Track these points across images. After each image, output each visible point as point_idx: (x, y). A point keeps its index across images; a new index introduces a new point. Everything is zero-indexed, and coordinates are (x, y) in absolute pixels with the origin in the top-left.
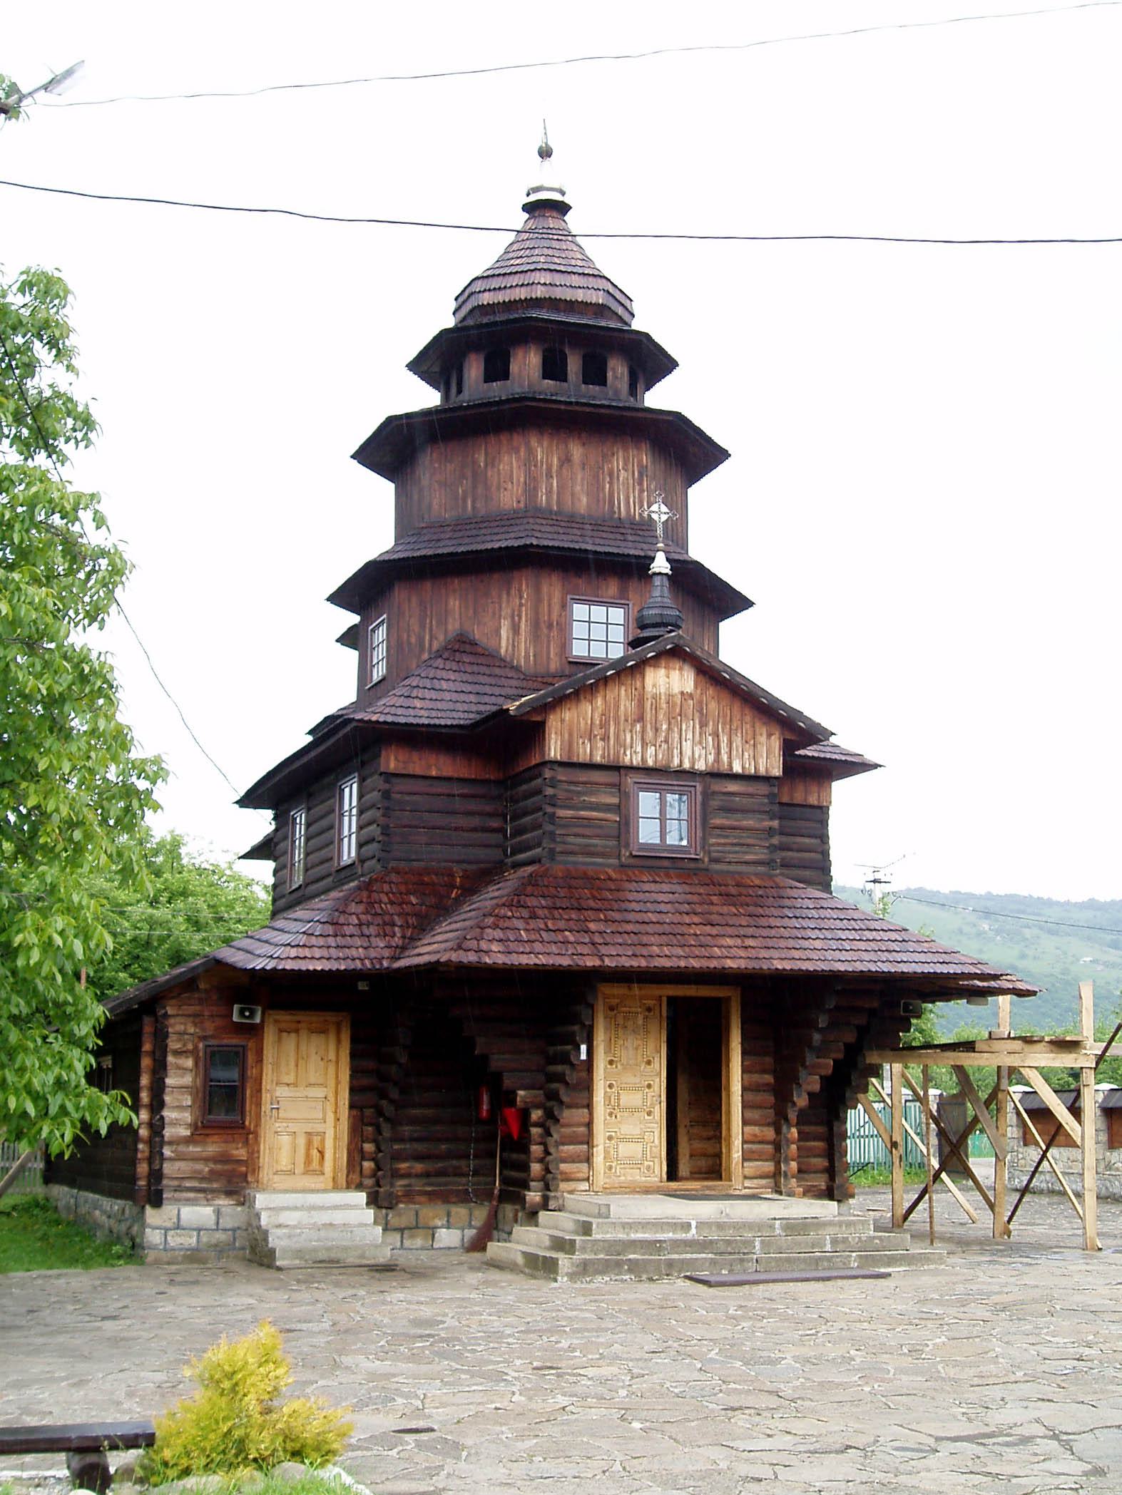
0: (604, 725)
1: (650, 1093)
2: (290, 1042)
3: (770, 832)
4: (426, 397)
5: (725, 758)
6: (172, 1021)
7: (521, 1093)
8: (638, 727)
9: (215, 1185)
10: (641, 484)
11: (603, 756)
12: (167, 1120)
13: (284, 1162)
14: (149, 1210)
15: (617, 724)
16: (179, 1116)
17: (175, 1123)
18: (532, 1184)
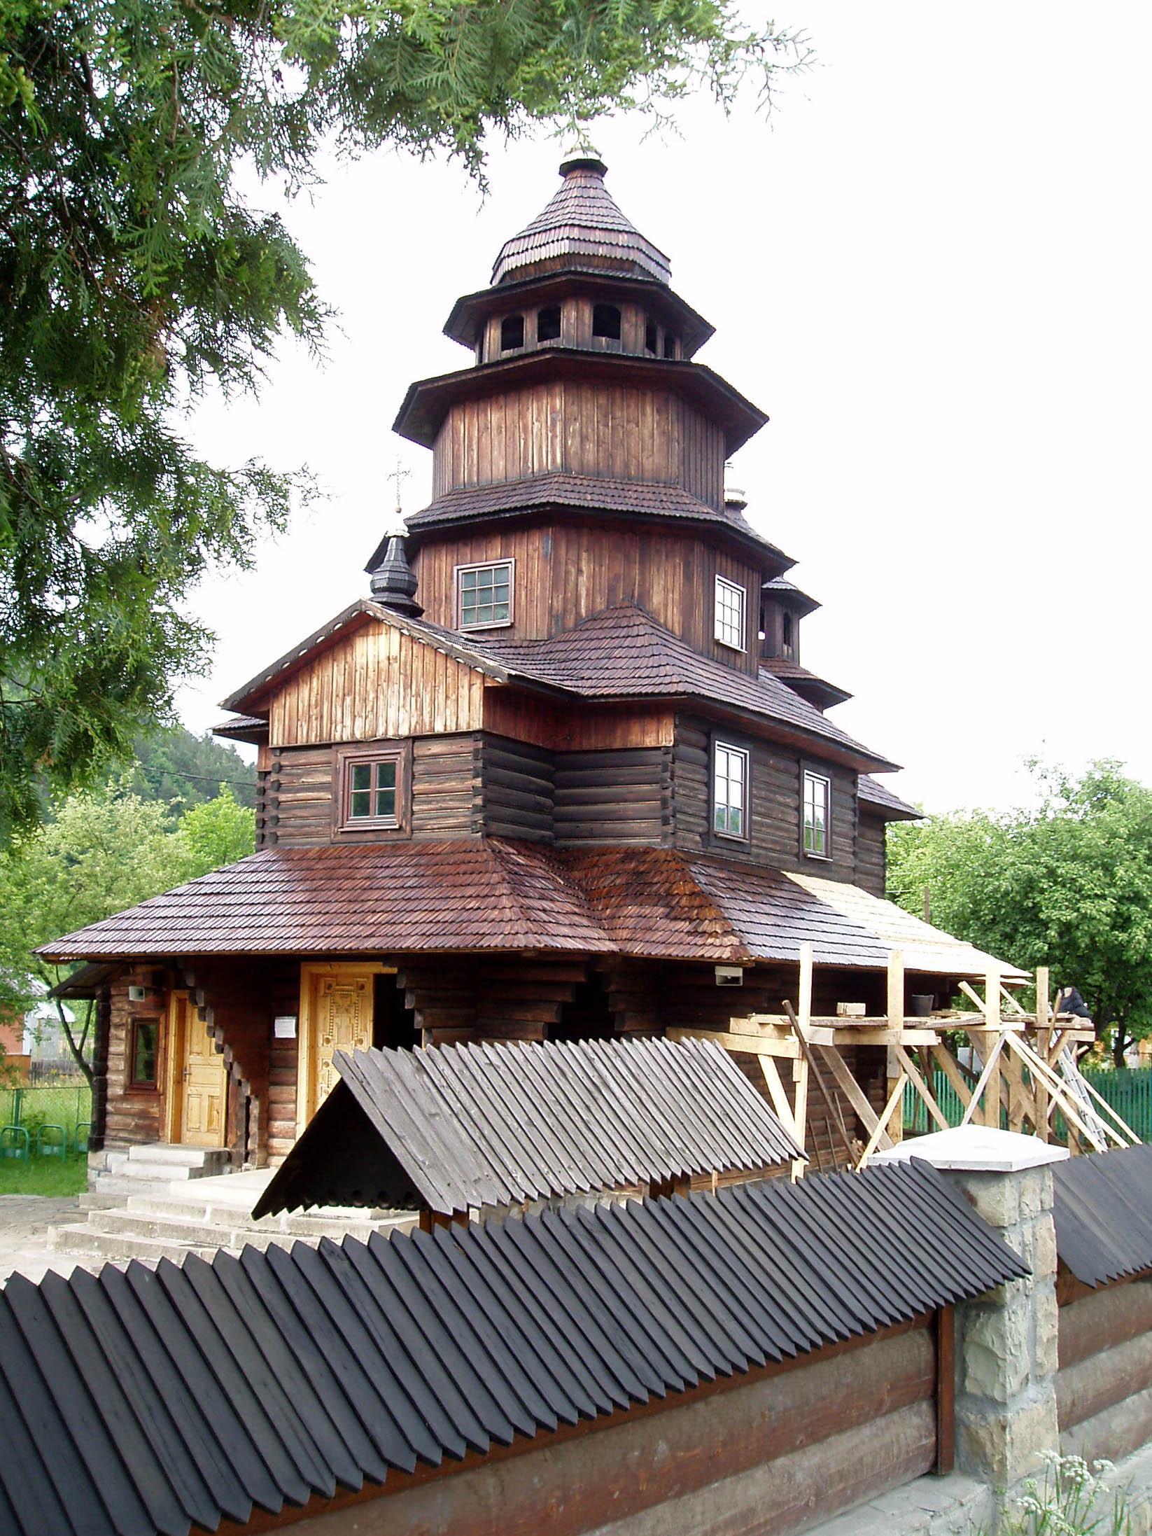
4: (461, 358)
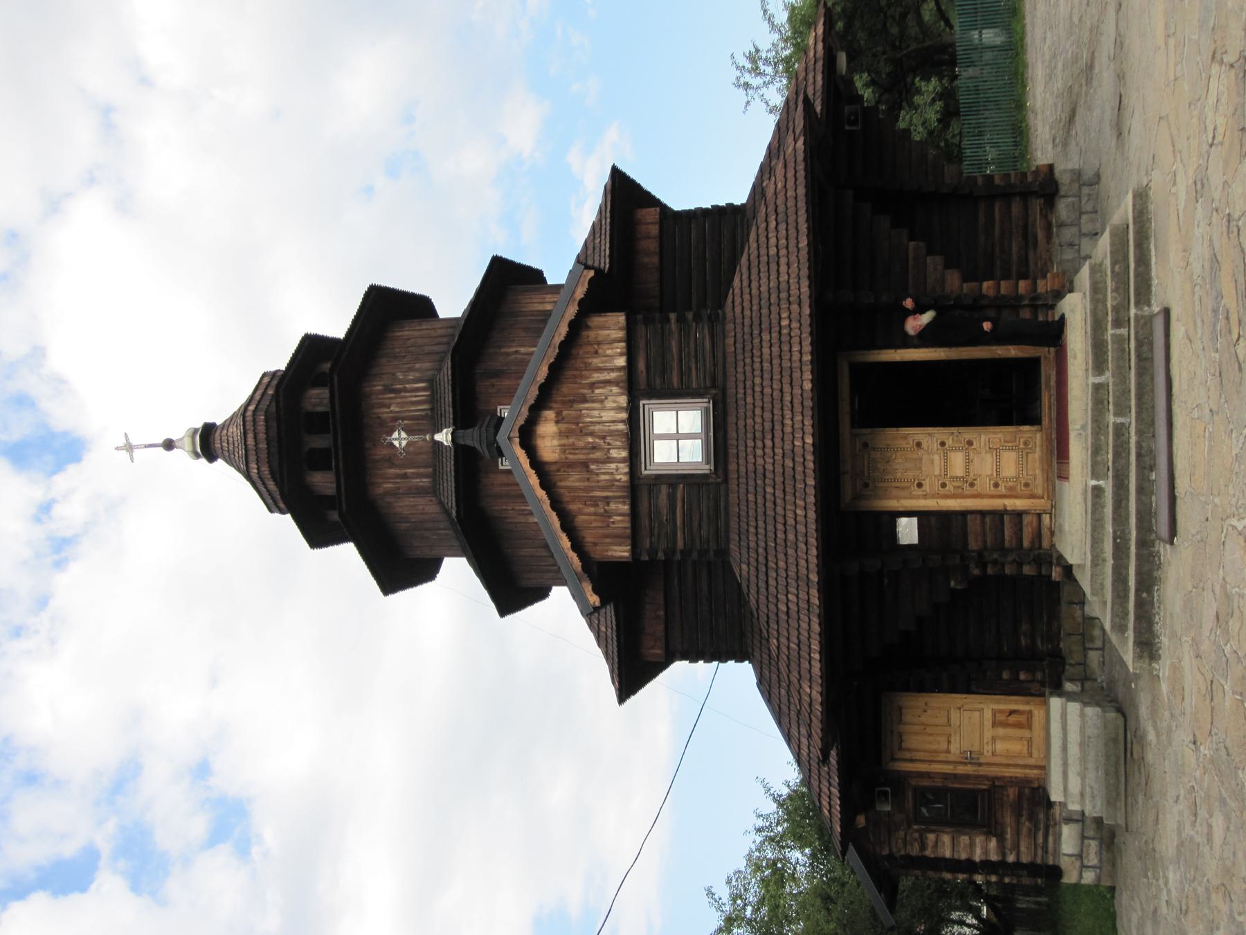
0: (595, 502)
1: (949, 442)
2: (912, 741)
3: (681, 320)
5: (613, 375)
6: (894, 850)
7: (952, 584)
8: (593, 467)
9: (1041, 816)
10: (399, 391)
11: (624, 503)
12: (984, 858)
13: (1017, 747)
14: (1065, 880)
15: (591, 489)
16: (982, 848)
17: (986, 852)
18: (1044, 572)
